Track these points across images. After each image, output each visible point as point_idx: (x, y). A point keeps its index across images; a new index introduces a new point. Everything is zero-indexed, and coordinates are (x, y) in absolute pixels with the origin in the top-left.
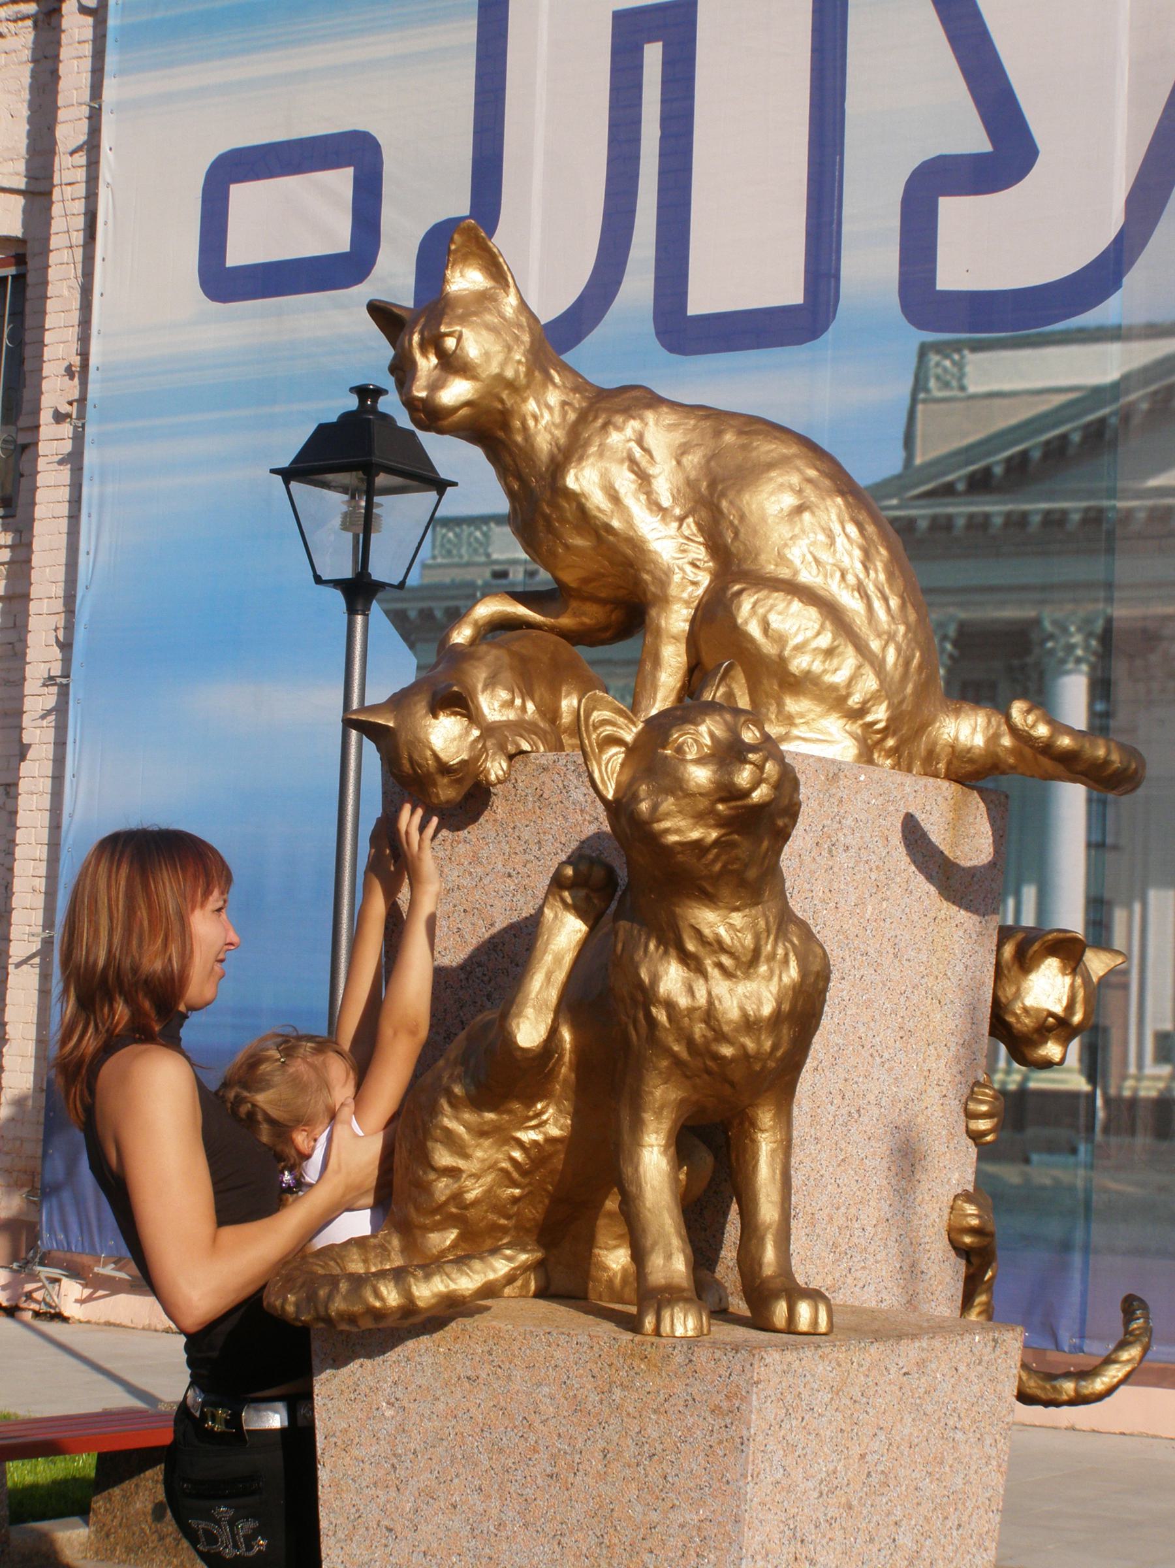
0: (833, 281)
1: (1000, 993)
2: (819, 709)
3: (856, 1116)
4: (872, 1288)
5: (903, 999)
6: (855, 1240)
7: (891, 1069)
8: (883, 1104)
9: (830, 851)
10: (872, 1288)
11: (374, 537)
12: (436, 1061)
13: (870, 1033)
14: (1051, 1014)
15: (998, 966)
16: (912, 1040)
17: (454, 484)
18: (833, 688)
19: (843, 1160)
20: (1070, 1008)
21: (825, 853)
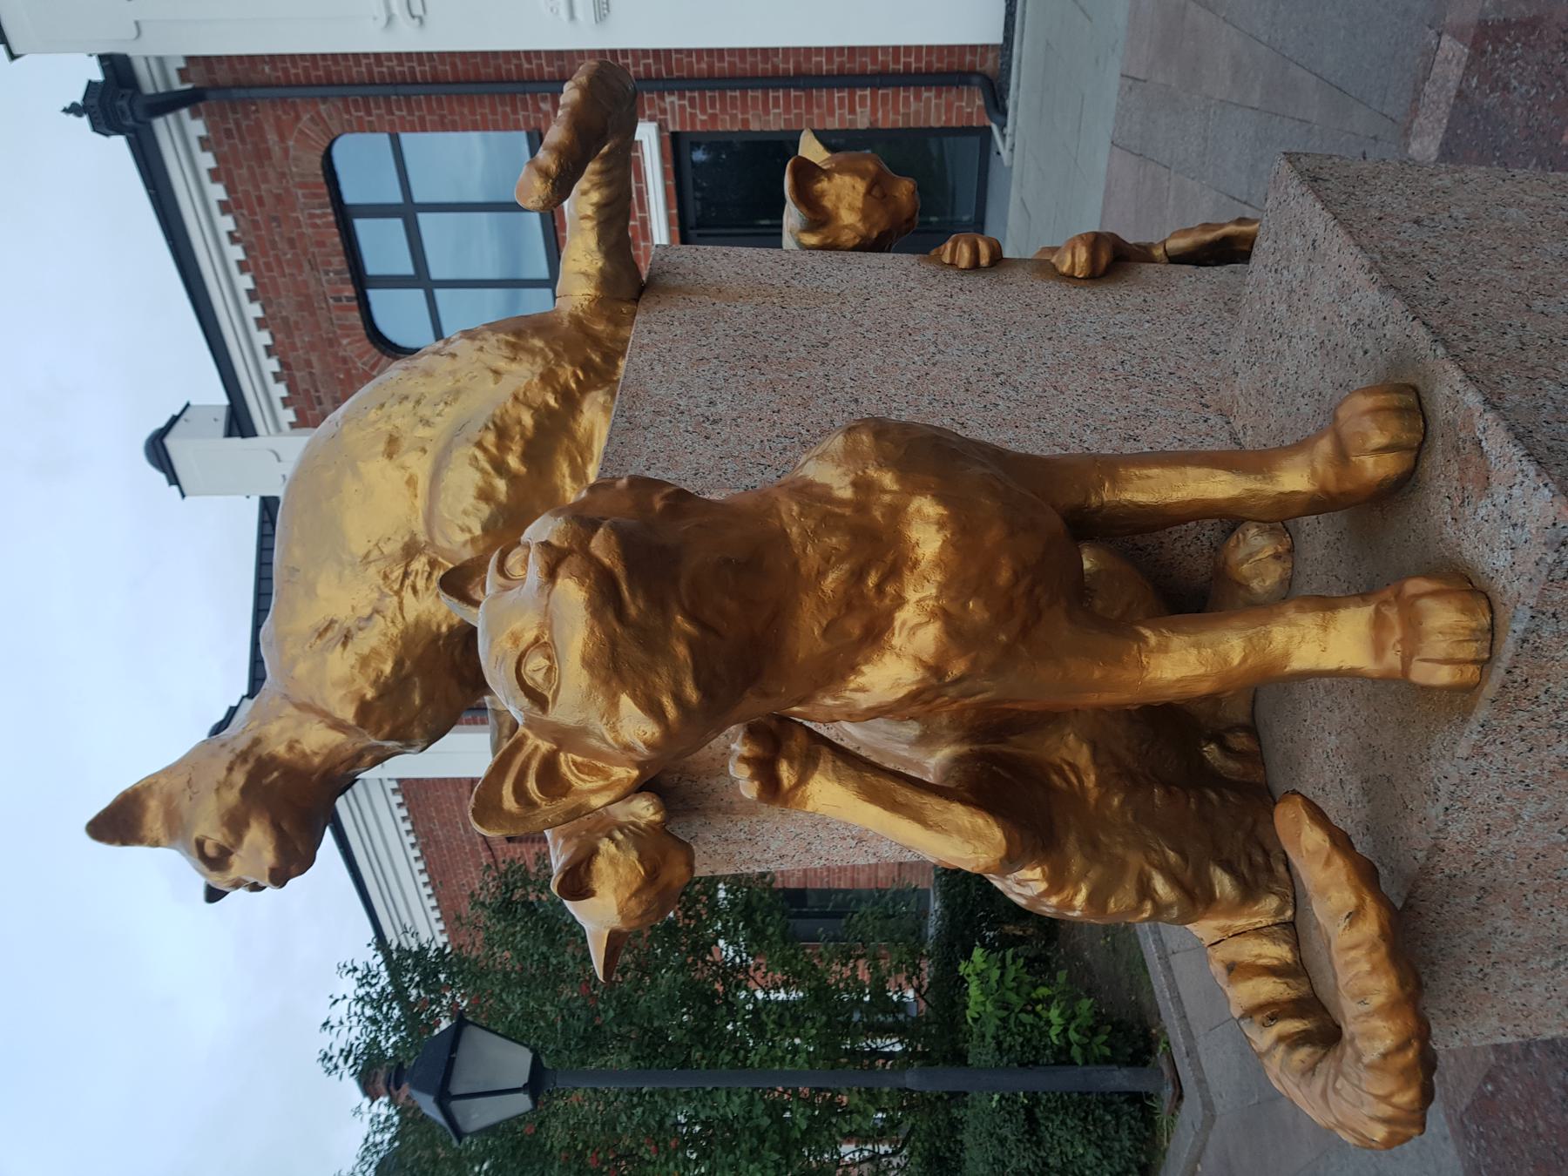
0: (694, 208)
1: (851, 244)
2: (566, 441)
3: (1002, 377)
4: (1181, 349)
5: (869, 335)
6: (1136, 370)
7: (946, 344)
8: (983, 349)
9: (715, 422)
10: (1181, 349)
11: (370, 934)
12: (1020, 914)
13: (912, 367)
14: (868, 192)
15: (822, 247)
16: (911, 324)
17: (65, 110)
18: (538, 425)
19: (1055, 388)
20: (861, 174)
21: (718, 427)
